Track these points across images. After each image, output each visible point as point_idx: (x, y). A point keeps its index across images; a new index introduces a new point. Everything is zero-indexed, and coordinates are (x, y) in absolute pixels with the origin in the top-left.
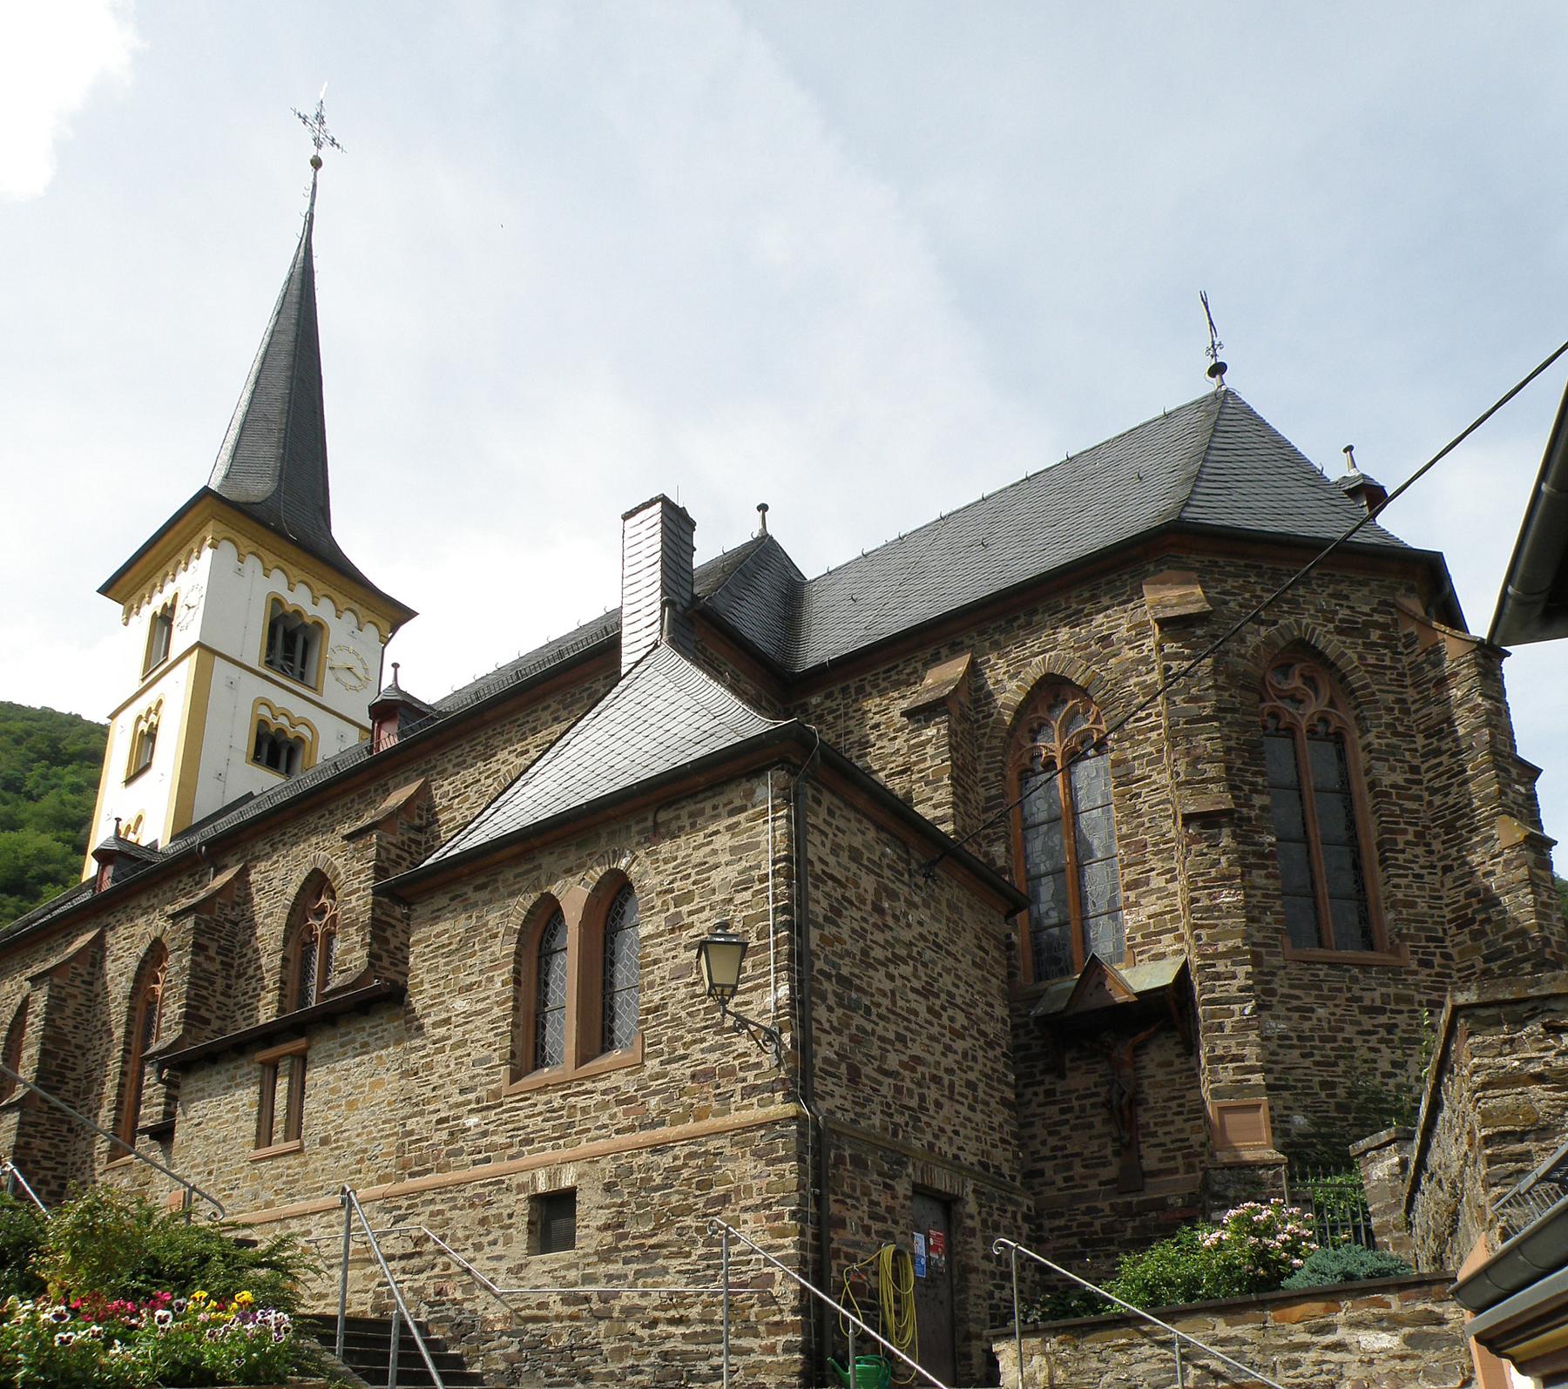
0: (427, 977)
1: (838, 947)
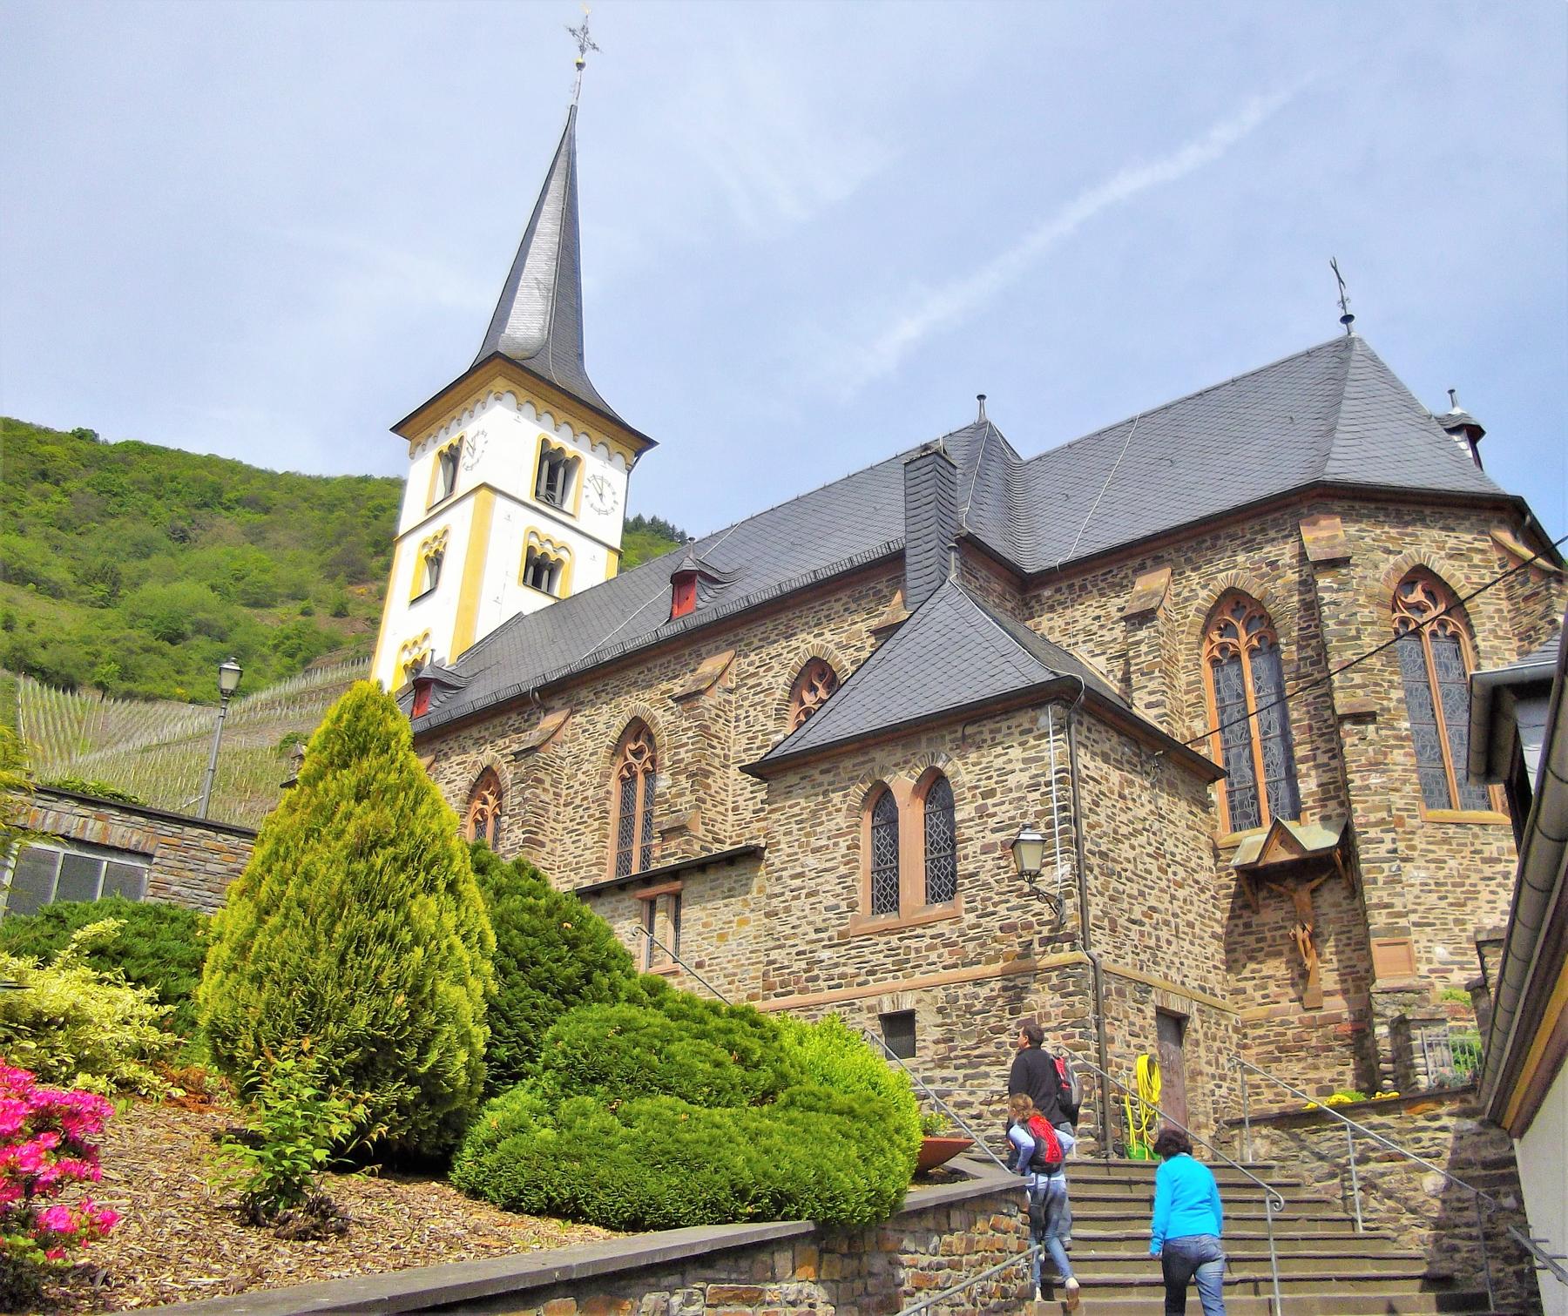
0: (784, 839)
1: (1098, 831)
